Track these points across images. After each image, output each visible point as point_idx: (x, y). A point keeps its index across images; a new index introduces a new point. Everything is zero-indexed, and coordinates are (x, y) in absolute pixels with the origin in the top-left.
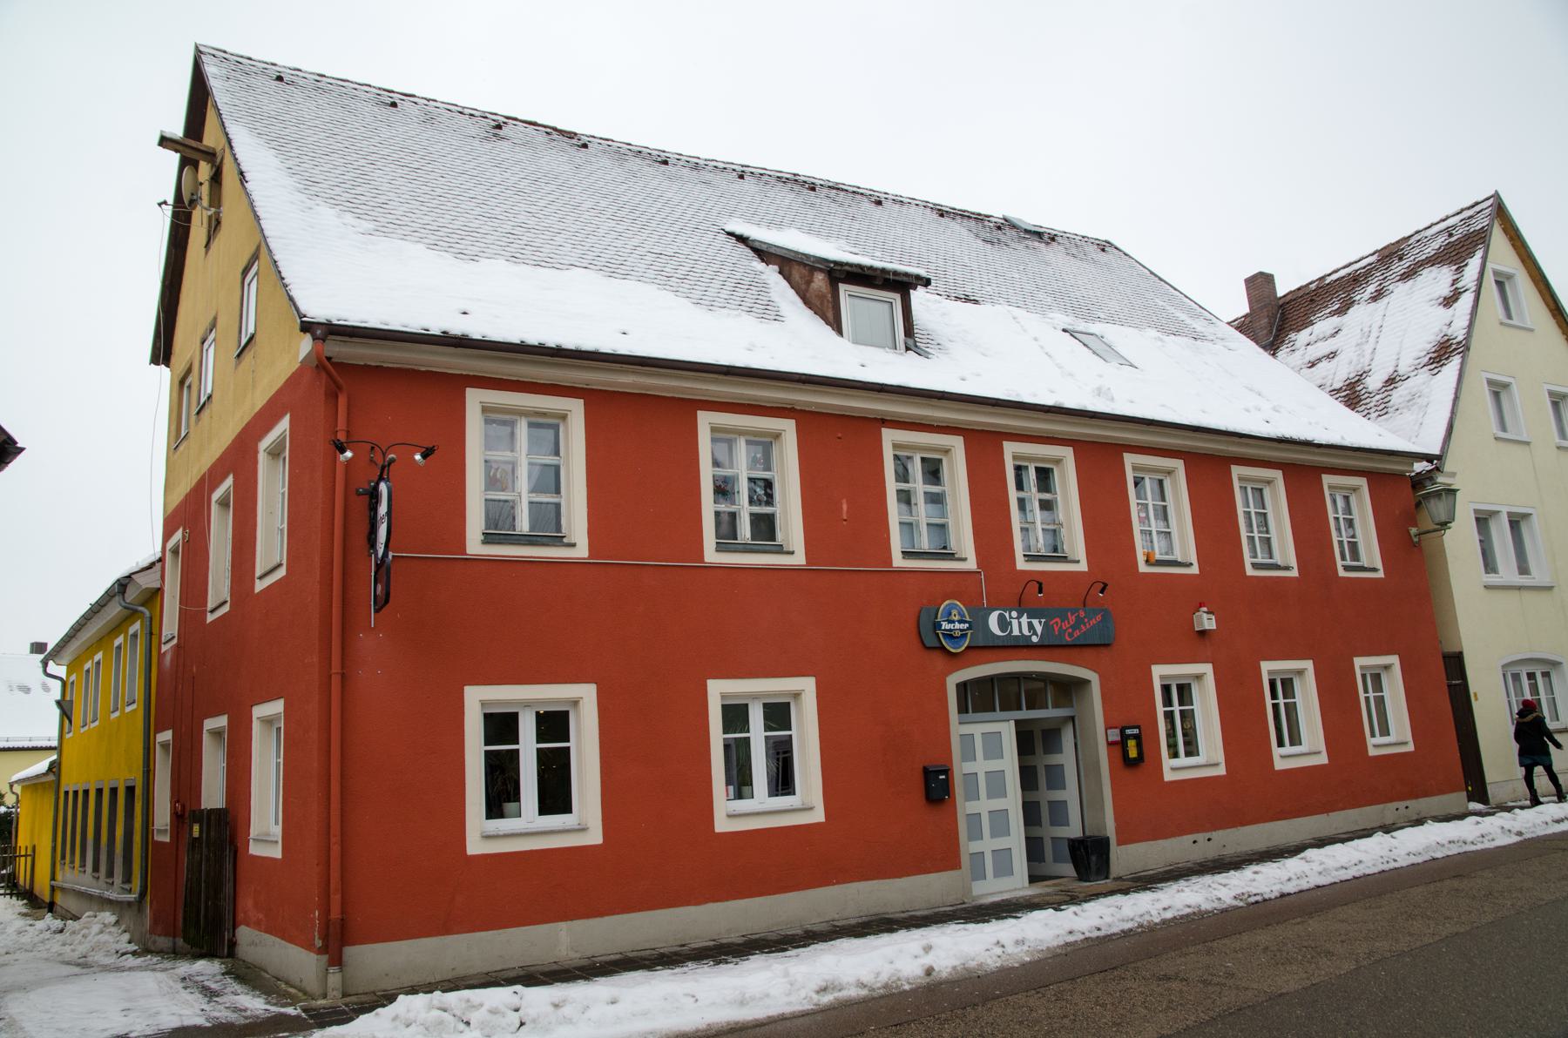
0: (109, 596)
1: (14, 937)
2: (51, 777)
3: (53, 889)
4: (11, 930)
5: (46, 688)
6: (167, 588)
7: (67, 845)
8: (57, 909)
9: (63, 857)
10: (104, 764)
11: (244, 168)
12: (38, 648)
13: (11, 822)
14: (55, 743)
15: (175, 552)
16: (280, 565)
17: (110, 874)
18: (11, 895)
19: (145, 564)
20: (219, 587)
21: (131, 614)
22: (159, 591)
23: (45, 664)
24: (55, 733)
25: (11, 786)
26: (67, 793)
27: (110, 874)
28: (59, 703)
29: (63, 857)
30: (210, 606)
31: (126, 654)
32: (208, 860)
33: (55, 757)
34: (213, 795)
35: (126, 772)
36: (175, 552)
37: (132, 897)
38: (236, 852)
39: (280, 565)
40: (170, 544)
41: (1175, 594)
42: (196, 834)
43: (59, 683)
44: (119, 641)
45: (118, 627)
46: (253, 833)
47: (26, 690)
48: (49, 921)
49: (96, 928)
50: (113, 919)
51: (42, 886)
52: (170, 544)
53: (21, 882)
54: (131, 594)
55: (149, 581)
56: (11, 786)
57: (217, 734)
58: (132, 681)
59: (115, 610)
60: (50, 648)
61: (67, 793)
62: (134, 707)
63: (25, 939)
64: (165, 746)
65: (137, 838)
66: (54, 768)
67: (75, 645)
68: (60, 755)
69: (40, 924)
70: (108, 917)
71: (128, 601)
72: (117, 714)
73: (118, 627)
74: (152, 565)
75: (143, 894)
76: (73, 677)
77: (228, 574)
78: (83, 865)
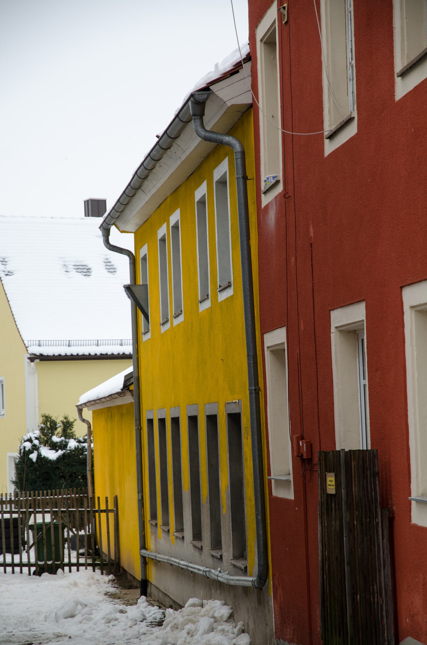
0: (181, 121)
1: (102, 626)
2: (129, 399)
3: (144, 561)
4: (98, 616)
5: (111, 268)
6: (260, 105)
7: (159, 498)
8: (151, 589)
9: (154, 516)
10: (200, 382)
11: (6, 293)
12: (94, 207)
13: (83, 462)
14: (128, 349)
15: (269, 42)
16: (350, 120)
17: (217, 544)
18: (94, 566)
19: (228, 66)
20: (339, 96)
21: (215, 149)
22: (251, 109)
23: (106, 232)
24: (127, 334)
25: (80, 411)
26: (150, 422)
27: (217, 544)
28: (128, 289)
29: (154, 516)
30: (328, 127)
31: (212, 210)
32: (350, 530)
33: (130, 369)
34: (351, 431)
35: (227, 394)
36: (269, 42)
37: (248, 580)
38: (391, 520)
39: (350, 120)
40: (261, 32)
41: (4, 501)
42: (331, 489)
43: (126, 259)
44: (201, 191)
45: (198, 171)
46: (416, 490)
47: (85, 271)
48: (142, 608)
49: (204, 623)
50: (224, 611)
51: (131, 557)
52: (261, 32)
53: (105, 549)
54: (213, 117)
55: (234, 94)
56: (80, 411)
57: (351, 332)
58: (224, 253)
59: (191, 143)
60: (109, 206)
61: (150, 422)
62: (229, 293)
63: (117, 631)
64: (277, 352)
65: (249, 492)
66: (131, 384)
67: (142, 200)
68: (137, 367)
69: (133, 612)
70: (219, 608)
71: (209, 127)
72: (207, 304)
73: (198, 171)
74: (236, 69)
75: (263, 577)
76: (144, 251)
77: (352, 73)
78: (180, 529)
